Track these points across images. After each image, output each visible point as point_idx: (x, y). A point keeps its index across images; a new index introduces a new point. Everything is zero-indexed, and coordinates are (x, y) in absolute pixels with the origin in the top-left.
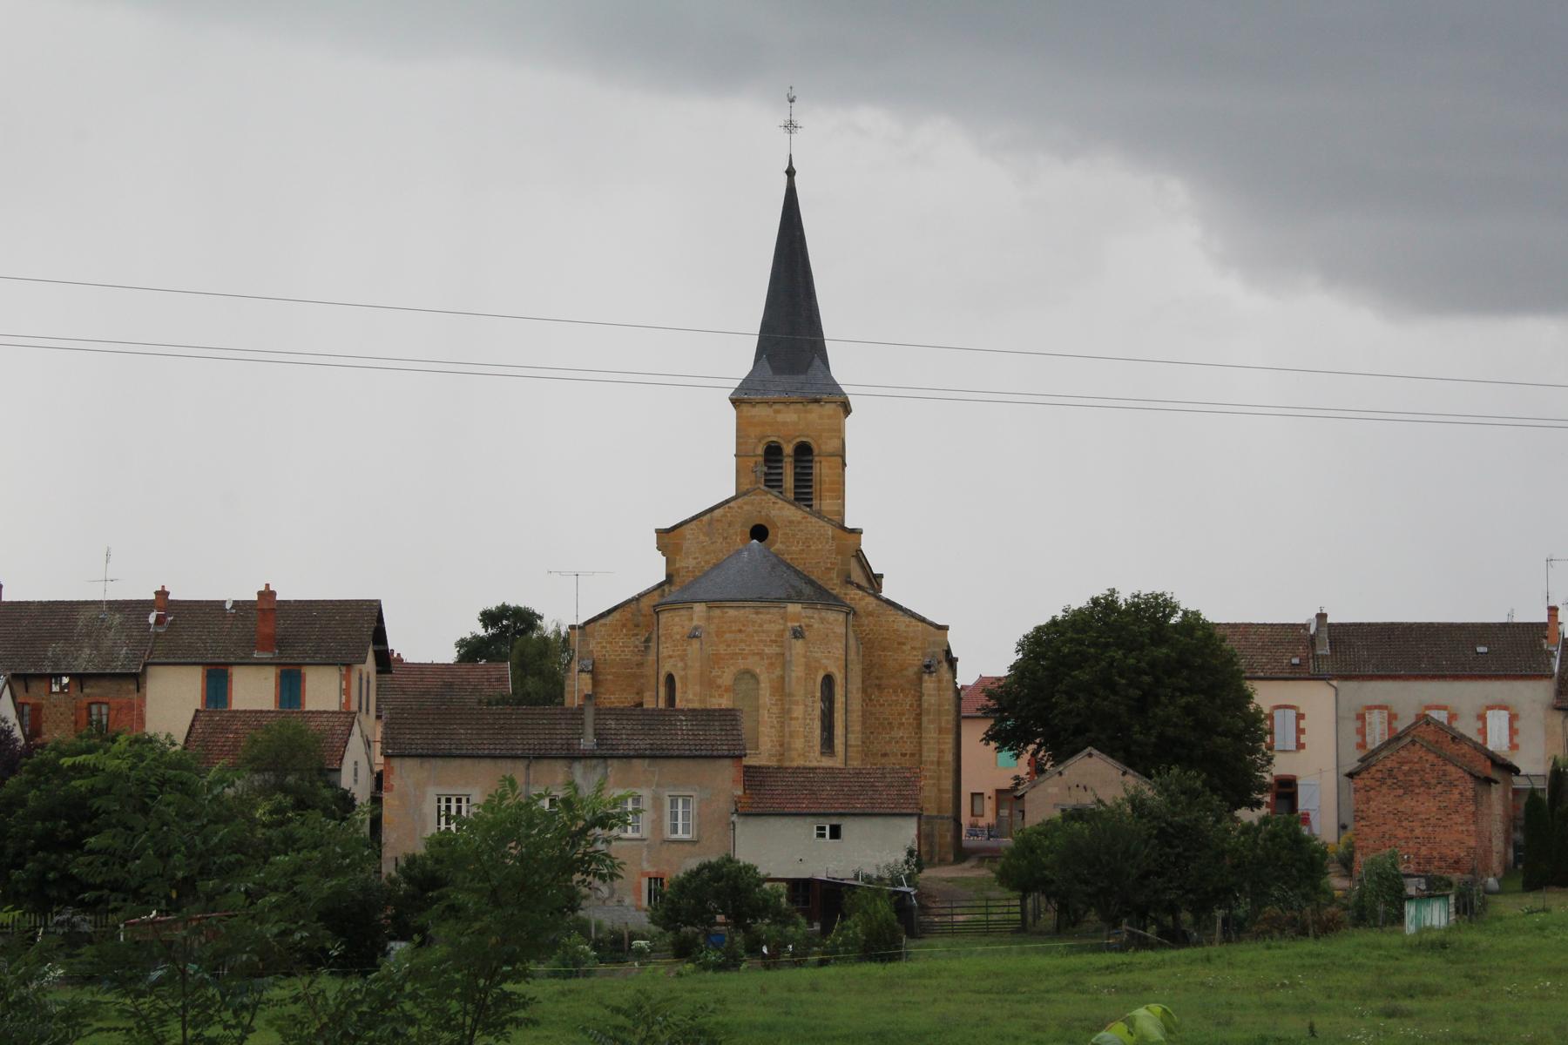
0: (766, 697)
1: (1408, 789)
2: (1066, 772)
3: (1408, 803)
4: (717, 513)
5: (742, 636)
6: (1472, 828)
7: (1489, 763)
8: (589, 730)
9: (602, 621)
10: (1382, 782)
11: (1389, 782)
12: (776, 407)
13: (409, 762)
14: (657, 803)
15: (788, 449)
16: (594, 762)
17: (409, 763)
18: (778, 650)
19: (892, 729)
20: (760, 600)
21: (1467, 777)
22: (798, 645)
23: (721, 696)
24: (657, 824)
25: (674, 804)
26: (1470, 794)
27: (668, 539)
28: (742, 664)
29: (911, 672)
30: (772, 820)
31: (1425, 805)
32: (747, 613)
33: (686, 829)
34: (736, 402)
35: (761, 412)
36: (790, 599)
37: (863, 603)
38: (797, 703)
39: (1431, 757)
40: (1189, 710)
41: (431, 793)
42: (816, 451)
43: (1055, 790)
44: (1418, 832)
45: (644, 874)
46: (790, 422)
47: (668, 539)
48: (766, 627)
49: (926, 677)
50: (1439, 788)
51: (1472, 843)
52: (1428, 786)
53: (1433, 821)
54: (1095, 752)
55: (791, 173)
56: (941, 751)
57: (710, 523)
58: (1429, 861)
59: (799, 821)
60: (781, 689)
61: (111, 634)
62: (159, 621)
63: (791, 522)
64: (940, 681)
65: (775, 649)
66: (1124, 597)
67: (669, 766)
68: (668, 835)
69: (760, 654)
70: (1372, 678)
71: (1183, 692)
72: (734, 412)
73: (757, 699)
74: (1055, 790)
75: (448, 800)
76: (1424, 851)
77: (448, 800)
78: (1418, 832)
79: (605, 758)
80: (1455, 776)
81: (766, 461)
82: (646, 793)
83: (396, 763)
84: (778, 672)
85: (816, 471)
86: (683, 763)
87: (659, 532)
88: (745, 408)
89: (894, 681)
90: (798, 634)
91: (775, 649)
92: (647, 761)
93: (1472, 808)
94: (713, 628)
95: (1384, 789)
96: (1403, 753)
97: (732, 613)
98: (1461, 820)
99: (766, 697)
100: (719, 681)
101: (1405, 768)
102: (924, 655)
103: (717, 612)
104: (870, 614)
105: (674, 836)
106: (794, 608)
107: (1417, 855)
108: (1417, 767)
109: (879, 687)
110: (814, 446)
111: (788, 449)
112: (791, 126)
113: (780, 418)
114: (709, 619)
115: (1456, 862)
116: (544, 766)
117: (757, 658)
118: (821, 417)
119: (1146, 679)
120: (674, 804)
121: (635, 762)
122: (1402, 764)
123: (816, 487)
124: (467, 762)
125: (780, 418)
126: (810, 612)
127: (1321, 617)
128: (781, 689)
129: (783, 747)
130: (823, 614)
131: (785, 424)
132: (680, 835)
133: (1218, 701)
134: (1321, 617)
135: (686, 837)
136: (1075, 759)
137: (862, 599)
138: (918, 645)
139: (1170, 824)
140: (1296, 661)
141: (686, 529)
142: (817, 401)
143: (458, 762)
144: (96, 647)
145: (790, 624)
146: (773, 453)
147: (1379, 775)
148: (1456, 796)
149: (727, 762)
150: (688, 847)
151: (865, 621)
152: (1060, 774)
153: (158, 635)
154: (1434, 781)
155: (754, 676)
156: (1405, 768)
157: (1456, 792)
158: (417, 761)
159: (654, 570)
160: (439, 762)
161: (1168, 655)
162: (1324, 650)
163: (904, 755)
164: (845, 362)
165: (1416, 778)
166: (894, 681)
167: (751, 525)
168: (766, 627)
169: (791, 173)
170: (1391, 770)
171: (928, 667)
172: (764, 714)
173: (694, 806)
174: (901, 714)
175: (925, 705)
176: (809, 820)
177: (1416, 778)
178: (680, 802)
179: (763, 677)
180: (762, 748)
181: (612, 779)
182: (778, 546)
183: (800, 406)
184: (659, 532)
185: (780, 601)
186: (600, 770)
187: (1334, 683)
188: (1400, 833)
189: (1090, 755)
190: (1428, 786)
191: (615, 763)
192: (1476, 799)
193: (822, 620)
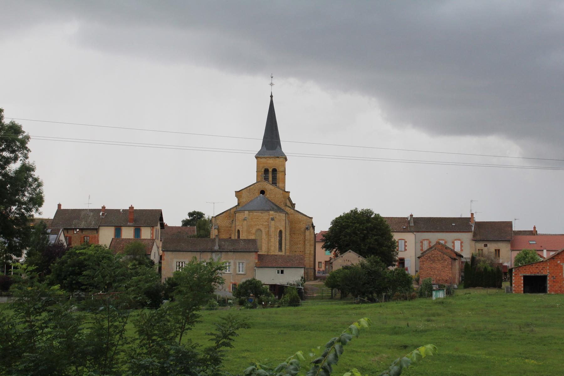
1: (434, 261)
3: (434, 265)
8: (217, 244)
10: (427, 259)
13: (169, 253)
14: (235, 264)
15: (270, 170)
22: (273, 222)
25: (239, 264)
26: (450, 263)
27: (238, 194)
28: (258, 227)
29: (303, 229)
31: (438, 266)
34: (256, 157)
35: (263, 160)
36: (270, 210)
45: (231, 283)
46: (271, 163)
47: (238, 194)
55: (272, 96)
58: (439, 280)
60: (268, 234)
61: (90, 218)
62: (103, 214)
69: (263, 225)
71: (375, 235)
76: (438, 278)
78: (436, 273)
79: (221, 252)
82: (232, 262)
83: (165, 253)
86: (242, 254)
88: (259, 159)
90: (273, 219)
91: (266, 223)
97: (255, 213)
99: (264, 236)
103: (251, 213)
104: (292, 214)
106: (271, 212)
111: (270, 170)
113: (268, 162)
114: (249, 215)
119: (365, 232)
120: (239, 264)
121: (229, 253)
123: (278, 180)
126: (276, 213)
128: (268, 234)
132: (241, 272)
134: (411, 216)
142: (278, 157)
143: (182, 253)
146: (266, 171)
148: (446, 263)
149: (254, 253)
151: (290, 216)
155: (261, 230)
159: (234, 202)
162: (412, 224)
164: (286, 147)
169: (272, 96)
177: (436, 259)
185: (268, 210)
186: (220, 255)
188: (432, 273)
193: (279, 216)
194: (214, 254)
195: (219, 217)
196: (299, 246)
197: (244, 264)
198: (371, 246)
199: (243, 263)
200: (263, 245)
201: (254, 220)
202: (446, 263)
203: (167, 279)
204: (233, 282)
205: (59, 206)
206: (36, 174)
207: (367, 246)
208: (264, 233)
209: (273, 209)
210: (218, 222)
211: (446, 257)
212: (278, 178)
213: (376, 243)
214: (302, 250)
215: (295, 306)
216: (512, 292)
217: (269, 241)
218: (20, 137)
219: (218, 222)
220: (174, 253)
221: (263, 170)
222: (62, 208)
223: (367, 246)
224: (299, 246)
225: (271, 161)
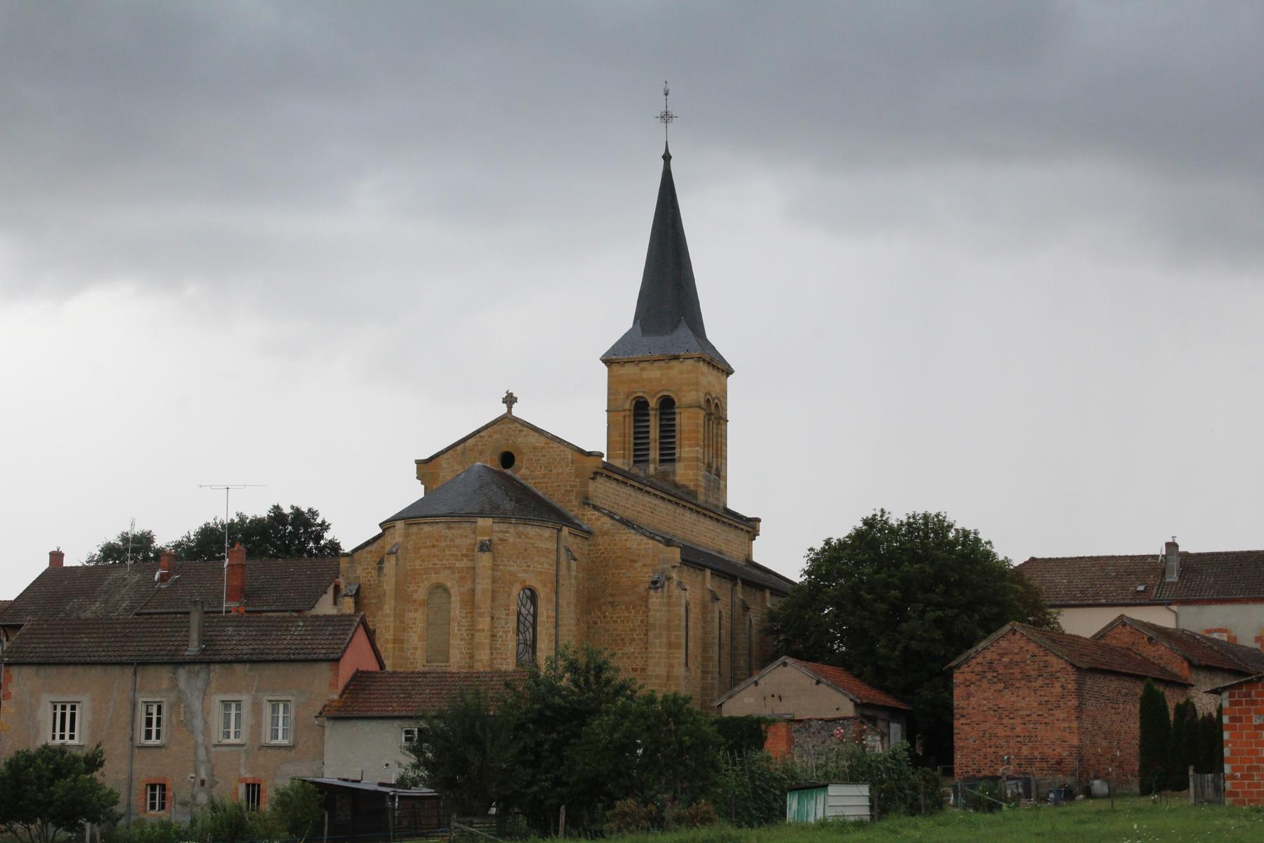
0: (456, 611)
2: (761, 682)
3: (1009, 697)
5: (435, 551)
7: (1186, 665)
8: (194, 635)
9: (368, 549)
11: (989, 675)
12: (642, 365)
14: (257, 707)
15: (653, 403)
16: (197, 667)
18: (470, 564)
19: (624, 644)
20: (451, 515)
21: (1069, 668)
22: (485, 559)
23: (416, 610)
24: (256, 729)
26: (1072, 686)
27: (426, 468)
28: (435, 578)
29: (642, 588)
32: (441, 529)
33: (237, 735)
34: (608, 360)
35: (629, 370)
36: (482, 514)
37: (599, 523)
38: (482, 615)
39: (1032, 647)
40: (938, 622)
41: (46, 700)
42: (677, 404)
47: (426, 468)
48: (457, 541)
49: (652, 592)
50: (1040, 682)
51: (1075, 742)
52: (1028, 678)
53: (1034, 717)
54: (789, 660)
55: (667, 158)
57: (463, 452)
58: (1030, 762)
59: (385, 725)
60: (470, 602)
61: (123, 591)
62: (163, 578)
63: (535, 448)
64: (669, 597)
66: (897, 516)
67: (269, 671)
68: (267, 740)
69: (451, 568)
70: (1210, 602)
72: (606, 369)
75: (64, 708)
76: (1025, 751)
77: (64, 708)
78: (1018, 730)
79: (209, 663)
80: (1056, 667)
82: (246, 699)
84: (469, 586)
85: (677, 422)
86: (283, 668)
87: (418, 462)
88: (615, 367)
89: (626, 598)
90: (484, 548)
95: (985, 683)
96: (1004, 644)
97: (427, 528)
98: (1062, 716)
99: (456, 611)
100: (415, 596)
101: (1006, 659)
102: (654, 572)
103: (415, 528)
104: (605, 533)
105: (274, 742)
106: (483, 523)
107: (1018, 755)
108: (1017, 658)
109: (612, 604)
110: (676, 399)
111: (653, 403)
112: (666, 117)
113: (645, 375)
114: (407, 535)
115: (1059, 763)
116: (151, 672)
117: (448, 572)
118: (681, 373)
121: (238, 667)
122: (1002, 655)
123: (677, 440)
124: (80, 669)
125: (645, 375)
126: (504, 527)
127: (1172, 546)
130: (521, 528)
132: (280, 740)
133: (977, 617)
134: (1172, 546)
136: (770, 667)
137: (597, 519)
140: (1141, 588)
141: (442, 460)
142: (676, 358)
143: (71, 669)
145: (479, 538)
146: (641, 407)
147: (979, 669)
148: (1057, 688)
149: (324, 667)
150: (283, 752)
152: (756, 683)
153: (159, 590)
154: (1034, 674)
155: (446, 590)
156: (1006, 659)
157: (1058, 685)
162: (1173, 578)
163: (635, 670)
164: (719, 328)
165: (1016, 671)
166: (626, 598)
167: (500, 452)
168: (457, 541)
169: (667, 158)
170: (991, 663)
171: (654, 583)
172: (455, 628)
173: (292, 714)
174: (633, 630)
175: (651, 620)
176: (397, 723)
177: (1016, 671)
178: (233, 705)
179: (454, 591)
180: (452, 660)
182: (524, 471)
183: (662, 364)
184: (418, 462)
185: (470, 516)
186: (203, 675)
187: (1174, 608)
188: (1000, 731)
189: (785, 664)
190: (1028, 678)
192: (1079, 693)
193: (519, 535)
194: (182, 673)
195: (364, 552)
198: (914, 645)
199: (239, 707)
200: (454, 642)
201: (423, 551)
202: (1057, 688)
203: (297, 783)
205: (56, 557)
206: (305, 509)
207: (900, 647)
208: (455, 600)
209: (494, 512)
211: (1056, 663)
213: (938, 635)
216: (1221, 803)
221: (628, 405)
222: (68, 562)
223: (900, 647)
225: (653, 373)
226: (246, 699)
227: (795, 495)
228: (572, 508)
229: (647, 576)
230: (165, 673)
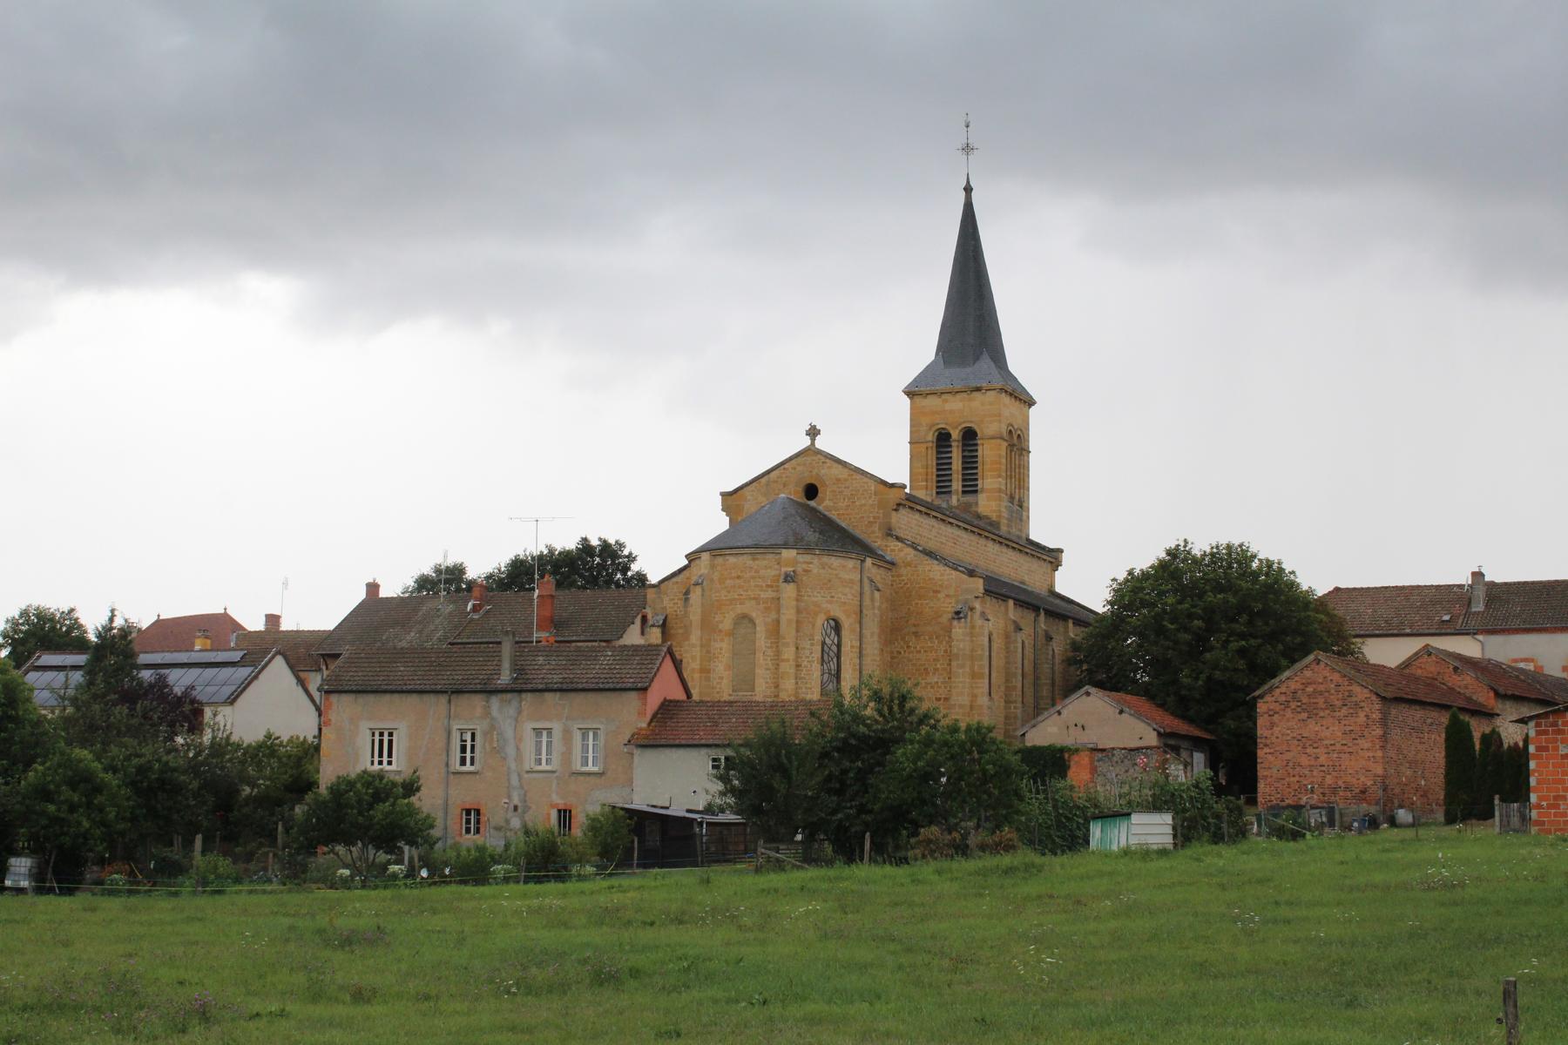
0: (762, 640)
1: (1311, 712)
2: (1065, 712)
3: (1313, 727)
4: (773, 474)
6: (1379, 754)
7: (1492, 694)
8: (506, 665)
10: (1286, 704)
11: (1293, 705)
13: (345, 698)
14: (567, 733)
15: (956, 435)
16: (509, 696)
17: (346, 699)
18: (774, 595)
20: (756, 547)
21: (1374, 697)
22: (789, 590)
24: (567, 757)
25: (585, 737)
26: (1376, 716)
27: (731, 500)
28: (740, 609)
29: (945, 619)
30: (667, 751)
31: (1329, 730)
32: (746, 560)
34: (910, 393)
35: (932, 402)
36: (786, 546)
40: (1242, 652)
43: (1054, 730)
44: (1323, 759)
45: (553, 806)
46: (956, 412)
47: (731, 500)
49: (955, 623)
50: (1344, 711)
54: (1092, 690)
55: (968, 189)
56: (974, 696)
57: (767, 484)
58: (1334, 791)
60: (775, 631)
61: (437, 621)
63: (838, 480)
65: (770, 594)
66: (1200, 546)
68: (578, 767)
71: (1242, 636)
73: (754, 642)
74: (1054, 730)
75: (381, 734)
76: (1329, 780)
77: (381, 734)
78: (1323, 759)
79: (520, 691)
80: (1360, 697)
81: (938, 446)
82: (557, 727)
83: (334, 698)
84: (773, 616)
85: (979, 453)
86: (591, 696)
87: (723, 494)
88: (918, 399)
90: (788, 579)
91: (770, 594)
92: (558, 694)
93: (1379, 732)
94: (716, 576)
95: (1289, 713)
96: (1308, 673)
97: (732, 560)
98: (1366, 745)
99: (762, 640)
101: (1310, 689)
103: (720, 560)
105: (585, 769)
106: (788, 554)
108: (1321, 688)
109: (916, 634)
111: (956, 435)
112: (967, 149)
113: (948, 407)
114: (713, 567)
115: (1363, 792)
119: (1197, 623)
120: (585, 737)
121: (548, 696)
122: (1306, 685)
126: (808, 558)
127: (1478, 575)
128: (775, 631)
129: (746, 680)
130: (825, 559)
131: (952, 412)
132: (591, 768)
134: (1478, 575)
135: (596, 769)
138: (952, 592)
139: (854, 736)
140: (1446, 618)
142: (978, 389)
143: (387, 697)
144: (420, 632)
146: (943, 438)
147: (1283, 698)
148: (1362, 718)
149: (633, 694)
150: (592, 779)
151: (903, 571)
152: (1059, 713)
154: (1338, 703)
155: (752, 621)
156: (1310, 689)
157: (1362, 715)
158: (351, 697)
160: (371, 698)
161: (1226, 601)
163: (938, 699)
168: (762, 572)
169: (968, 189)
171: (958, 613)
172: (760, 655)
176: (704, 751)
177: (1321, 701)
181: (525, 713)
184: (723, 494)
185: (774, 547)
186: (515, 703)
187: (1480, 637)
188: (1304, 761)
189: (1088, 694)
191: (528, 697)
192: (1384, 722)
194: (495, 701)
196: (933, 679)
197: (601, 734)
198: (1218, 674)
204: (560, 802)
206: (612, 541)
210: (666, 602)
211: (1360, 693)
212: (979, 459)
213: (1242, 664)
214: (942, 693)
215: (477, 882)
217: (778, 659)
218: (1255, 565)
219: (666, 602)
220: (362, 699)
223: (1203, 677)
224: (933, 679)
226: (557, 727)
227: (1097, 529)
228: (876, 540)
229: (949, 607)
230: (478, 701)
